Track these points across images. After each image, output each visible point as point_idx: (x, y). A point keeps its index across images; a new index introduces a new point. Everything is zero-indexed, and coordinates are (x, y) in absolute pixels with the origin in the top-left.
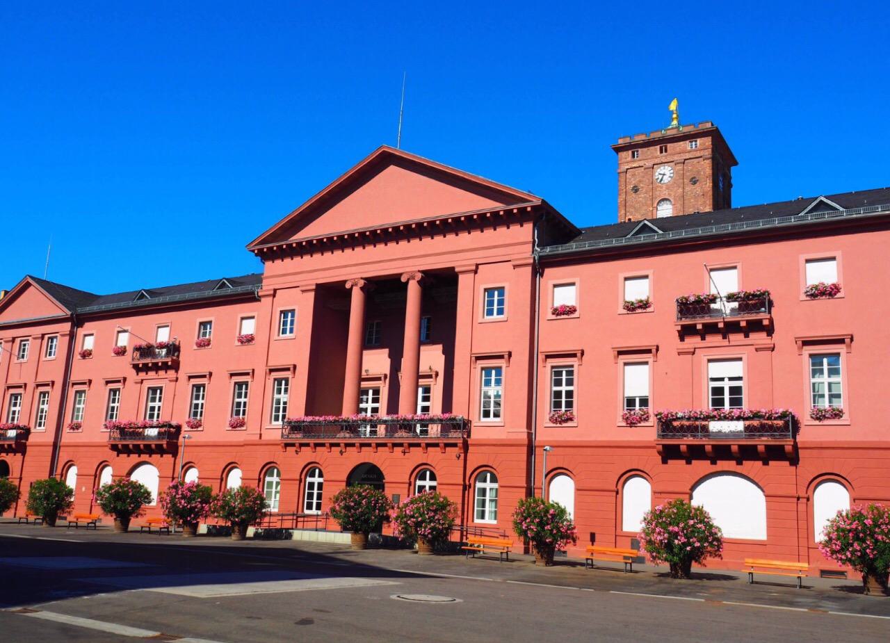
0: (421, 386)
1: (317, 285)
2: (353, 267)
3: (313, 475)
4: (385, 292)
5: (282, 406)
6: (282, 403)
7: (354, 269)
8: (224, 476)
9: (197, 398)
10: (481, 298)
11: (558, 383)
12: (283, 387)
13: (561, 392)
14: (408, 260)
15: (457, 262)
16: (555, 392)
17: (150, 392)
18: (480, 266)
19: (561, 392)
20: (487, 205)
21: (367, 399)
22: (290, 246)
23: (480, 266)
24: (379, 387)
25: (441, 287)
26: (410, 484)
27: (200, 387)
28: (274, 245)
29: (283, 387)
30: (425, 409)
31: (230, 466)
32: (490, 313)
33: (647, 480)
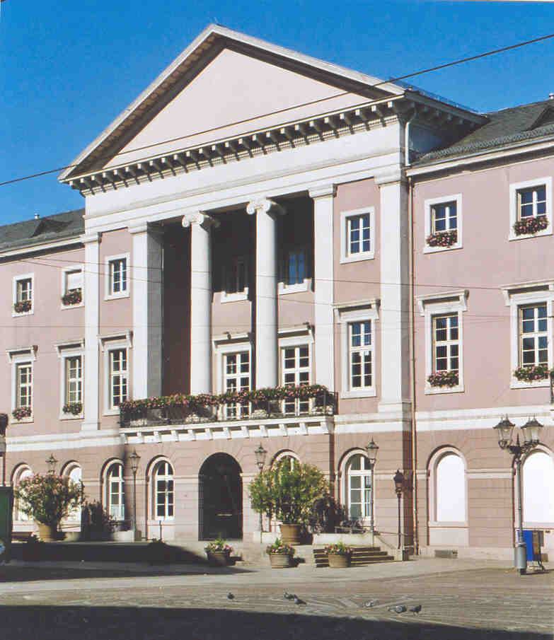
0: (282, 348)
1: (149, 224)
2: (191, 197)
3: (357, 467)
4: (231, 228)
5: (363, 363)
6: (363, 359)
7: (134, 213)
8: (431, 467)
9: (117, 367)
10: (344, 230)
11: (441, 336)
12: (362, 334)
13: (445, 348)
14: (253, 184)
15: (314, 183)
16: (439, 348)
17: (69, 362)
18: (339, 187)
19: (445, 348)
20: (354, 101)
21: (235, 367)
22: (110, 173)
23: (339, 187)
24: (308, 345)
25: (294, 215)
26: (102, 481)
27: (75, 360)
28: (92, 175)
29: (362, 334)
30: (290, 378)
31: (69, 466)
32: (355, 249)
33: (545, 452)
